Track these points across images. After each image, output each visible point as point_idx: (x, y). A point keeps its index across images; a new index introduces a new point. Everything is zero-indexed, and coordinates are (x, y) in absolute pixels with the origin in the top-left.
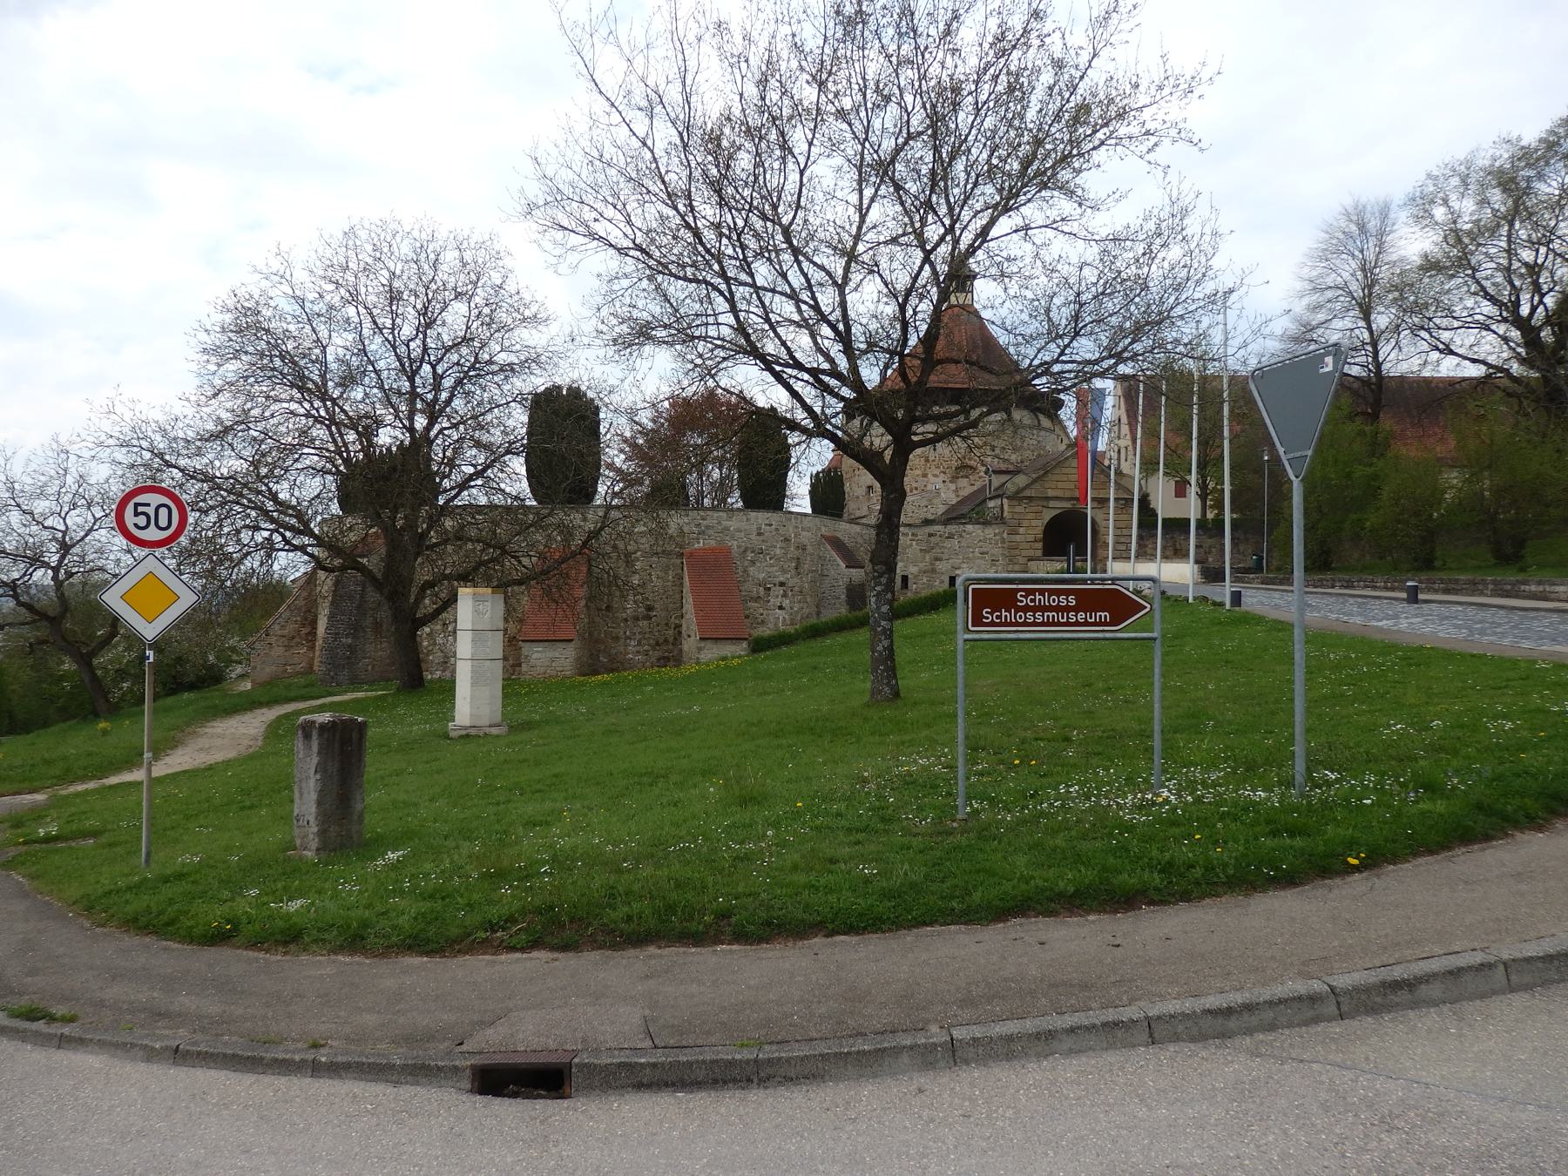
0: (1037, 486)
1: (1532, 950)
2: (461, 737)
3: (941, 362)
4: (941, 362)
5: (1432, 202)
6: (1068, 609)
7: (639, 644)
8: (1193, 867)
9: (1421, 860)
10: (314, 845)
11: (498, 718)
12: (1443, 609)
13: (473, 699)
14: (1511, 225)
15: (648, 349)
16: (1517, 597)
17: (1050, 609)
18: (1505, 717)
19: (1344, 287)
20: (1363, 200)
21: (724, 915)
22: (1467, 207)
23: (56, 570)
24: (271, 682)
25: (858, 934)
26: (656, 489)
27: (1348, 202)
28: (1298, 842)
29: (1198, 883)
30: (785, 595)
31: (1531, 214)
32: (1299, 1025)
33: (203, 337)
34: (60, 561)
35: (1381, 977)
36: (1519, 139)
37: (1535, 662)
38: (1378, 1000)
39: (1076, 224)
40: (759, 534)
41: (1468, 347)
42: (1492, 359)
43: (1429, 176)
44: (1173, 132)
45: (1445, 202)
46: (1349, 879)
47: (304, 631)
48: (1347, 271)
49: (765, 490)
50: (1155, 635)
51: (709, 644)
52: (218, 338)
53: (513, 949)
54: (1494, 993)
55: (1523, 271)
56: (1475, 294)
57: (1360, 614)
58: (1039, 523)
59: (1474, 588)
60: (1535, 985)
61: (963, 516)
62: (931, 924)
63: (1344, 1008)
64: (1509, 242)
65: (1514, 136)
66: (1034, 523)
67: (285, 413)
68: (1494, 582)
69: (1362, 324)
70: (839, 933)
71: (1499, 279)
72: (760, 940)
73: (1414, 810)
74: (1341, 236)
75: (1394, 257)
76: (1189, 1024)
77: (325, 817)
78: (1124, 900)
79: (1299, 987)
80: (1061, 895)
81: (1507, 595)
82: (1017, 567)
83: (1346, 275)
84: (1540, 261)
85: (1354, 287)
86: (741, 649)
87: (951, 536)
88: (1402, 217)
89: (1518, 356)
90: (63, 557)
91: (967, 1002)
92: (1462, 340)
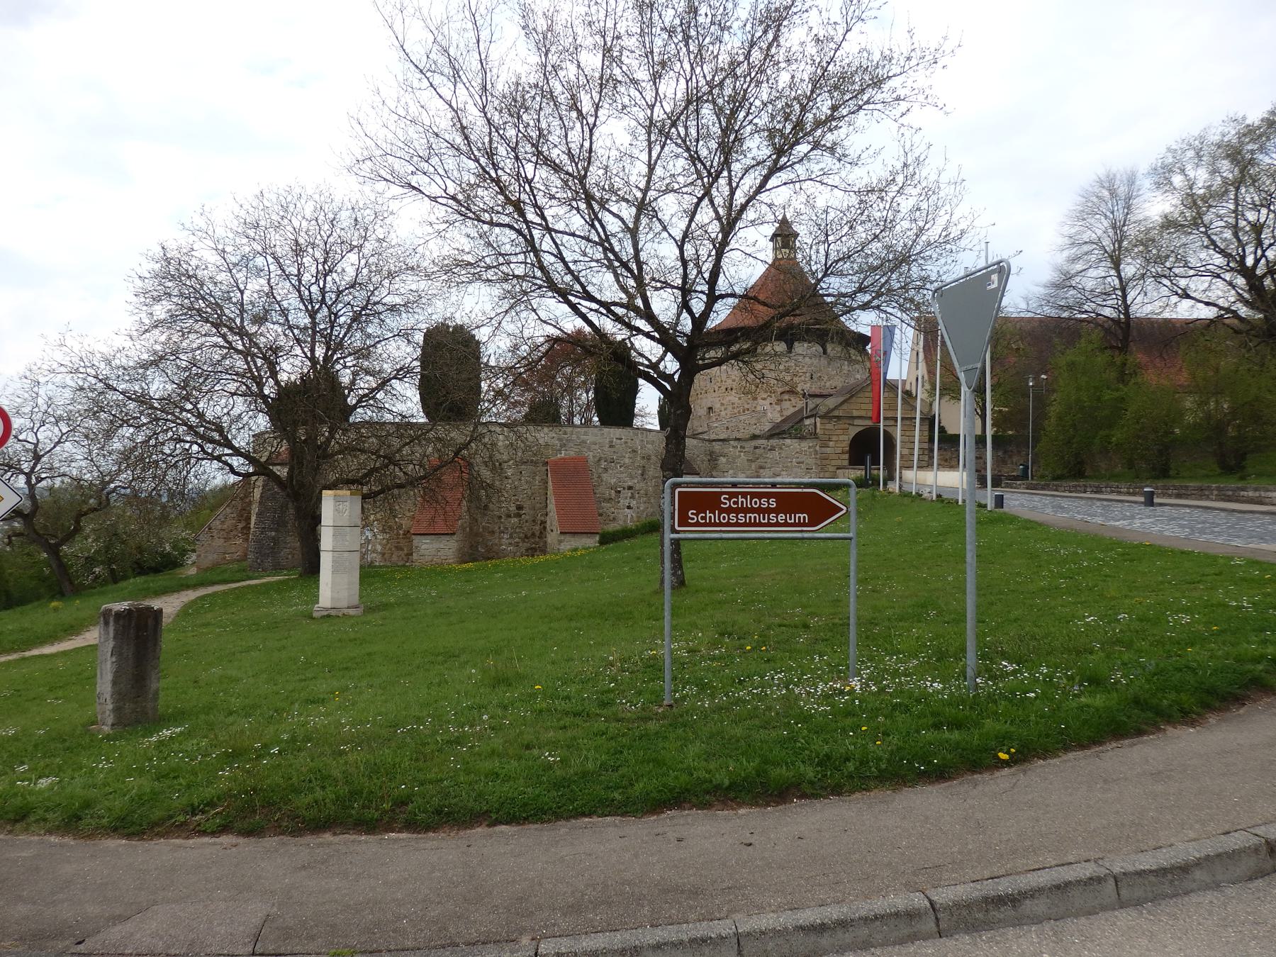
0: (845, 407)
1: (1147, 862)
2: (323, 617)
3: (722, 297)
4: (722, 297)
5: (1170, 171)
6: (769, 511)
7: (511, 537)
8: (848, 759)
9: (1071, 755)
10: (110, 721)
11: (356, 600)
12: (1174, 512)
13: (335, 586)
14: (1237, 189)
15: (477, 284)
16: (1237, 501)
17: (752, 510)
18: (1186, 610)
19: (1098, 242)
20: (1114, 170)
21: (402, 802)
22: (1201, 176)
23: (28, 476)
24: (214, 567)
25: (518, 824)
26: (534, 408)
27: (1102, 172)
28: (956, 736)
29: (851, 777)
30: (632, 497)
31: (1254, 181)
32: (894, 944)
33: (139, 283)
34: (33, 468)
35: (984, 892)
36: (1244, 118)
37: (1232, 559)
38: (980, 916)
39: (837, 177)
40: (611, 446)
41: (1200, 294)
42: (1221, 302)
43: (1169, 150)
44: (921, 98)
45: (1183, 171)
46: (997, 774)
47: (240, 526)
48: (1100, 228)
49: (616, 409)
50: (850, 535)
51: (568, 537)
52: (149, 285)
53: (203, 833)
54: (1104, 908)
55: (1248, 228)
56: (1207, 247)
57: (1102, 515)
58: (846, 438)
59: (1201, 493)
60: (1146, 900)
61: (784, 432)
62: (590, 815)
63: (943, 925)
64: (1237, 205)
65: (1240, 115)
66: (841, 438)
67: (203, 342)
68: (1218, 489)
69: (1113, 272)
70: (501, 823)
71: (1228, 234)
72: (427, 828)
73: (1074, 705)
74: (1095, 200)
75: (1141, 217)
76: (780, 941)
77: (120, 697)
78: (773, 793)
79: (898, 901)
80: (718, 787)
81: (1229, 499)
82: (827, 474)
83: (1099, 233)
84: (1262, 220)
85: (1106, 242)
86: (592, 542)
87: (773, 449)
88: (1146, 183)
89: (1241, 299)
90: (35, 465)
91: (575, 909)
92: (1198, 285)
